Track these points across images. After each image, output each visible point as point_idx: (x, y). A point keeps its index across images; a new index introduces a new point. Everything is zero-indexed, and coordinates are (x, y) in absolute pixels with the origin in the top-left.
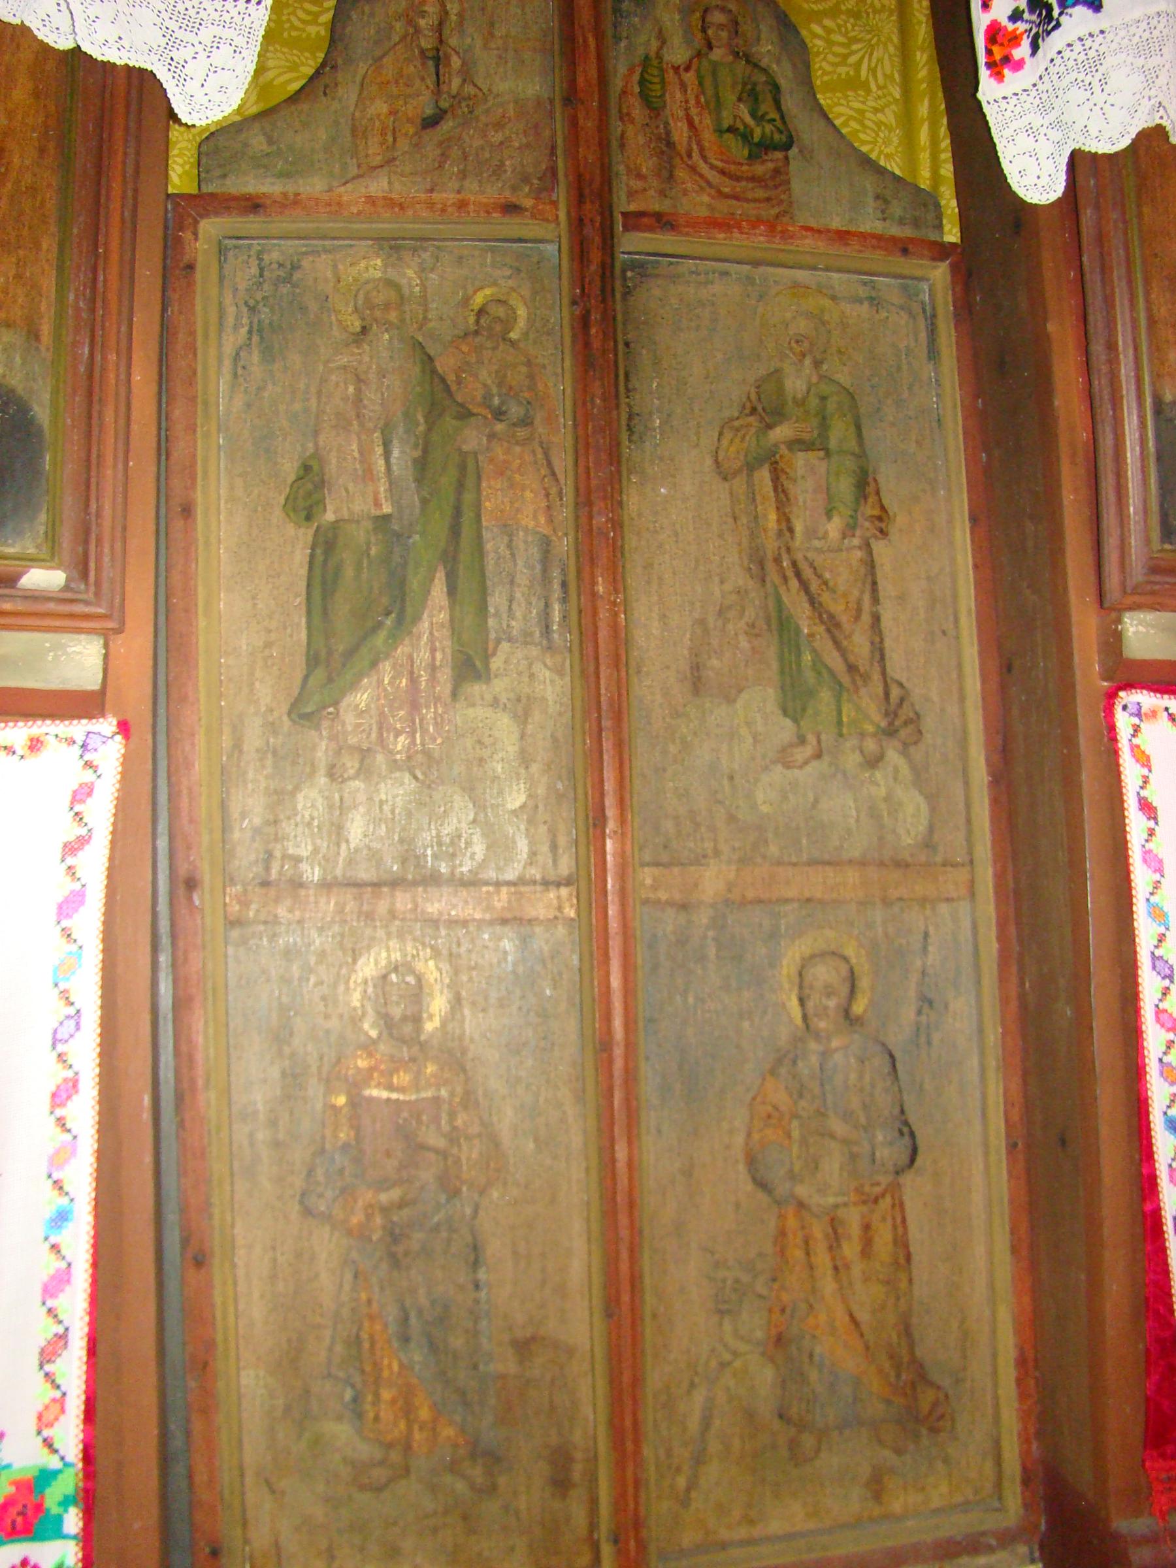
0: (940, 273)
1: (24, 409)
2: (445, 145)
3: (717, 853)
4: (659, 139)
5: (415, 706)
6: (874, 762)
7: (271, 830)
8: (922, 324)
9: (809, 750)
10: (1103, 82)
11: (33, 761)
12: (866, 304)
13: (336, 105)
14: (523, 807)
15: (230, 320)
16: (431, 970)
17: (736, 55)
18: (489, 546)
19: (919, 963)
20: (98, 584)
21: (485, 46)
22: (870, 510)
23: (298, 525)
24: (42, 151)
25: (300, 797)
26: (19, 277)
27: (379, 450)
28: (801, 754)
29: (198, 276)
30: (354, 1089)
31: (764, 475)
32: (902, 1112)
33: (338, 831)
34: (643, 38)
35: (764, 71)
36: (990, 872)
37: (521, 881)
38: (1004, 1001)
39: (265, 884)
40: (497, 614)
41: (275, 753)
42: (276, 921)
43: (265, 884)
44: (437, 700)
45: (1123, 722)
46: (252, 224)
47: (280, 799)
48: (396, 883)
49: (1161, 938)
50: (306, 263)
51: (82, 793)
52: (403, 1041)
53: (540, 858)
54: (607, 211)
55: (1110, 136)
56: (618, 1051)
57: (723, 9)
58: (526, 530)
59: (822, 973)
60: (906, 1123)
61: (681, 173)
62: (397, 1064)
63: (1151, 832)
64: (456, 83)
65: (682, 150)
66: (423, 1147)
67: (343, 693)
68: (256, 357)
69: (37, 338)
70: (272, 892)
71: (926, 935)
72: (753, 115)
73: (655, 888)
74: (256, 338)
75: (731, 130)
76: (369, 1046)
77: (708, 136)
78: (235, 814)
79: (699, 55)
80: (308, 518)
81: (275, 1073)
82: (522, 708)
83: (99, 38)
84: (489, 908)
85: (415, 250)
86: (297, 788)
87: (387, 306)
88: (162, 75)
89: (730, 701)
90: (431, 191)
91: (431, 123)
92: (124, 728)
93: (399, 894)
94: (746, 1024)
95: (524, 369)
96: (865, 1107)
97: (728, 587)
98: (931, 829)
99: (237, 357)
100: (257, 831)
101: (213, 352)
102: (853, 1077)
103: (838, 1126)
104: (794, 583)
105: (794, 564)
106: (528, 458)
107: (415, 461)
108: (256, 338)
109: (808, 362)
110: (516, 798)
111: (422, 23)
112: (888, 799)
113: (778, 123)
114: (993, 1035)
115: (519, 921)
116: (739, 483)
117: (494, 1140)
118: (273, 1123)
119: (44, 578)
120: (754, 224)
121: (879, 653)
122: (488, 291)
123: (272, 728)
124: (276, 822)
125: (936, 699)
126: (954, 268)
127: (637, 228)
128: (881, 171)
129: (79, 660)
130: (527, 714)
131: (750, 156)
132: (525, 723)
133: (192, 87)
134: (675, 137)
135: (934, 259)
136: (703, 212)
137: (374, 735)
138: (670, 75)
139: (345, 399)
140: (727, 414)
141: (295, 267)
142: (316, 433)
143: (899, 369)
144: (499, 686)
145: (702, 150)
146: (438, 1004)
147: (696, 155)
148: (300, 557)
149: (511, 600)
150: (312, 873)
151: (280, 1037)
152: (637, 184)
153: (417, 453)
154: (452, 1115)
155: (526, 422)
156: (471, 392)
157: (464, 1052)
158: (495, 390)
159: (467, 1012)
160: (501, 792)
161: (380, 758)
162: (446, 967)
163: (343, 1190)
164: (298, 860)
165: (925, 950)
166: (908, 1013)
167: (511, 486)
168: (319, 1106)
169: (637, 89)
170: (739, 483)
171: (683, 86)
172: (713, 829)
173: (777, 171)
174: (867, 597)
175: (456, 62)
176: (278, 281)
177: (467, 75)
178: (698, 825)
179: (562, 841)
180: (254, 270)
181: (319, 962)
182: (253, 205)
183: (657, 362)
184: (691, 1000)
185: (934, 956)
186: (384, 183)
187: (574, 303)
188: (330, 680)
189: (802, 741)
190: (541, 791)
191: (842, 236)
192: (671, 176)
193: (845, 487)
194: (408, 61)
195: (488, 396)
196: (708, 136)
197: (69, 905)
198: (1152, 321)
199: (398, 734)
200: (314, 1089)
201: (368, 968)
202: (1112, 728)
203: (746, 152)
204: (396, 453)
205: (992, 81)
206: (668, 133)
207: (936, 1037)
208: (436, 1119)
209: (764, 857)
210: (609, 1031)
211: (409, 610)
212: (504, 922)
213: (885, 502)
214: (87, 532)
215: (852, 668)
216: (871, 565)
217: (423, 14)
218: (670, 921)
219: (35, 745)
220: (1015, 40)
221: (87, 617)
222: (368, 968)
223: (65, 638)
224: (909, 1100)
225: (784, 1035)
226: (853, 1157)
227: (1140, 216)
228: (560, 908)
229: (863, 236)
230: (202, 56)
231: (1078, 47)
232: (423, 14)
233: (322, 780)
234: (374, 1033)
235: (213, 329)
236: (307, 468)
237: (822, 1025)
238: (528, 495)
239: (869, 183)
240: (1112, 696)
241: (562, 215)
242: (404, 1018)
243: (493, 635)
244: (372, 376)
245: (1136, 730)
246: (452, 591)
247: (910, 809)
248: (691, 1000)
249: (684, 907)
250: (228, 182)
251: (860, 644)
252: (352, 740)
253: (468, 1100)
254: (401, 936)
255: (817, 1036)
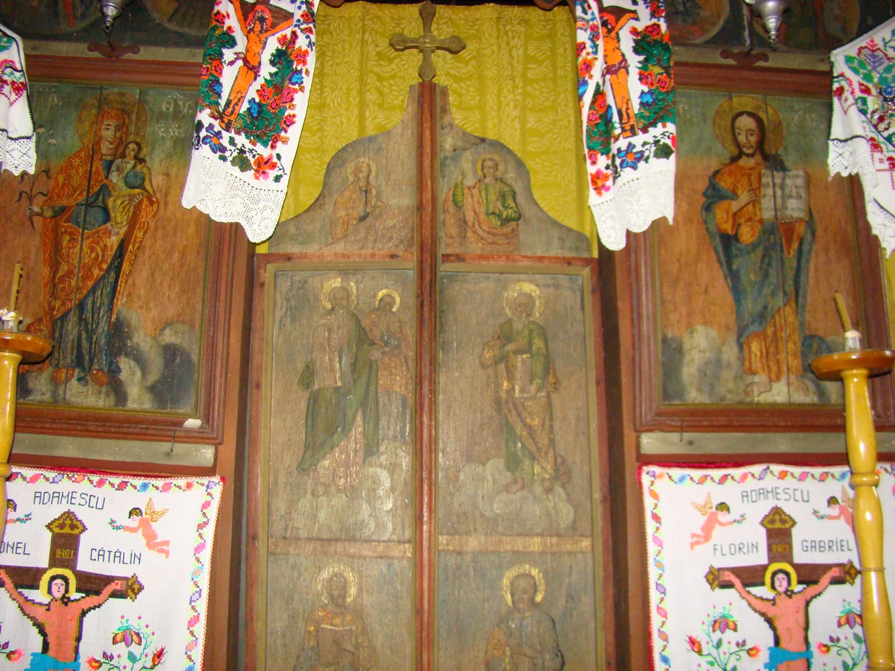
0: (586, 272)
1: (188, 356)
2: (368, 229)
3: (475, 530)
4: (460, 220)
5: (347, 466)
6: (549, 491)
7: (288, 516)
8: (578, 294)
9: (519, 486)
10: (638, 201)
11: (188, 492)
12: (552, 288)
13: (324, 213)
14: (391, 509)
15: (279, 305)
16: (350, 576)
17: (496, 179)
18: (380, 400)
19: (567, 580)
20: (212, 426)
21: (387, 184)
22: (551, 380)
23: (303, 391)
24: (199, 253)
25: (300, 503)
26: (188, 304)
27: (337, 359)
28: (514, 488)
29: (266, 288)
30: (317, 624)
31: (502, 366)
32: (558, 646)
33: (315, 517)
34: (455, 176)
35: (509, 186)
36: (600, 541)
37: (389, 541)
38: (606, 599)
39: (285, 538)
40: (383, 429)
41: (291, 485)
42: (288, 554)
43: (285, 538)
44: (357, 464)
45: (646, 479)
46: (288, 265)
47: (292, 504)
48: (337, 540)
49: (661, 576)
50: (310, 280)
51: (206, 505)
52: (338, 606)
53: (397, 532)
54: (434, 256)
55: (640, 226)
56: (426, 615)
57: (491, 160)
58: (396, 393)
59: (522, 583)
60: (560, 651)
61: (469, 234)
62: (336, 615)
63: (658, 529)
64: (374, 201)
65: (470, 224)
66: (345, 650)
67: (319, 461)
68: (289, 319)
69: (194, 328)
70: (288, 541)
71: (571, 568)
72: (503, 206)
73: (447, 545)
74: (289, 313)
75: (493, 213)
76: (324, 607)
77: (482, 217)
78: (274, 509)
79: (480, 181)
80: (308, 388)
81: (285, 616)
82: (393, 468)
83: (218, 214)
84: (375, 551)
85: (354, 274)
86: (299, 499)
87: (342, 299)
88: (243, 223)
89: (484, 465)
90: (362, 248)
91: (363, 219)
92: (223, 479)
93: (339, 545)
94: (486, 605)
95: (398, 324)
96: (540, 643)
97: (484, 415)
98: (575, 521)
99: (281, 321)
100: (283, 516)
101: (271, 319)
102: (535, 629)
103: (528, 651)
104: (514, 412)
105: (515, 405)
106: (398, 362)
107: (351, 365)
108: (289, 313)
109: (524, 315)
110: (389, 505)
111: (361, 175)
112: (555, 507)
113: (515, 209)
114: (601, 613)
115: (388, 557)
116: (491, 372)
117: (373, 649)
118: (284, 636)
119: (193, 423)
120: (500, 257)
121: (552, 442)
122: (384, 291)
123: (289, 474)
124: (290, 513)
125: (578, 463)
126: (592, 270)
127: (448, 261)
128: (561, 227)
129: (206, 454)
130: (394, 470)
131: (502, 225)
132: (393, 474)
133: (255, 226)
134: (468, 219)
135: (583, 266)
136: (479, 252)
137: (331, 478)
138: (466, 191)
139: (324, 338)
140: (486, 340)
141: (305, 282)
142: (312, 352)
143: (567, 316)
144: (383, 458)
145: (479, 223)
146: (353, 590)
147: (477, 226)
148: (304, 404)
149: (389, 422)
150: (303, 534)
151: (288, 601)
152: (449, 241)
153: (353, 360)
154: (357, 638)
155: (398, 347)
156: (376, 334)
157: (363, 611)
158: (385, 333)
159: (365, 594)
160: (382, 503)
161: (333, 488)
162: (356, 575)
163: (311, 666)
164: (298, 529)
165: (570, 574)
166: (562, 602)
167: (391, 374)
168: (303, 631)
169: (451, 199)
170: (491, 372)
171: (472, 196)
172: (474, 520)
173: (513, 230)
174: (547, 419)
175: (374, 192)
176: (298, 289)
177: (378, 198)
178: (467, 518)
179: (407, 524)
180: (289, 284)
181: (305, 571)
182: (289, 258)
183: (456, 319)
184: (462, 593)
185: (574, 577)
186: (343, 245)
187: (418, 297)
188: (314, 455)
189: (515, 481)
190: (399, 503)
191: (541, 259)
192: (465, 236)
193: (539, 369)
194: (355, 192)
195: (382, 336)
196: (482, 217)
197: (199, 549)
198: (663, 301)
199: (340, 478)
200: (301, 623)
201: (325, 574)
202: (640, 483)
203: (499, 223)
204: (344, 360)
205: (597, 196)
206: (464, 217)
207: (575, 613)
208: (351, 638)
209: (497, 532)
210: (422, 605)
211: (347, 426)
212: (381, 557)
213: (558, 376)
214: (209, 405)
215: (539, 449)
216: (549, 404)
217: (361, 172)
218: (452, 561)
219: (189, 486)
220: (606, 178)
221: (208, 439)
222: (325, 574)
223: (200, 446)
224: (561, 641)
225: (503, 610)
226: (535, 665)
227: (659, 255)
228: (405, 553)
229: (550, 258)
230: (259, 214)
231: (627, 185)
232: (361, 172)
233: (309, 496)
234: (326, 602)
235: (271, 311)
236: (308, 367)
237: (521, 606)
238: (398, 378)
239: (555, 233)
240: (640, 468)
241: (415, 258)
242: (339, 596)
243: (381, 437)
244: (335, 328)
245: (653, 483)
246: (364, 420)
247: (565, 511)
248: (462, 593)
249: (460, 553)
250: (280, 247)
251: (544, 441)
252: (322, 480)
253: (364, 631)
254: (339, 561)
255: (519, 610)
